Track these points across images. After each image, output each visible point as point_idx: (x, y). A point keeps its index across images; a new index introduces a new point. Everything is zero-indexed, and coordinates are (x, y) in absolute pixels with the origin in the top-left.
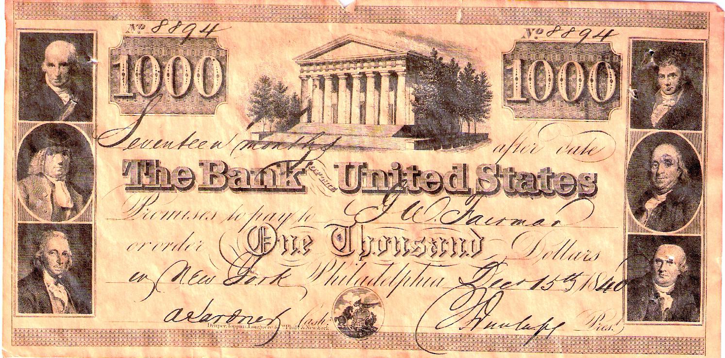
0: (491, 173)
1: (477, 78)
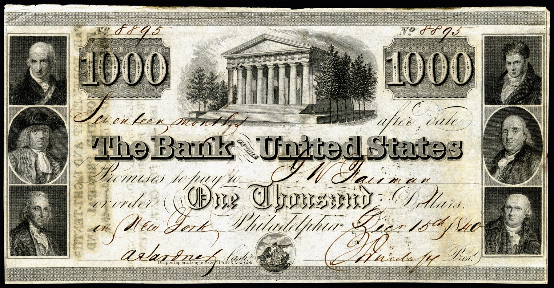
0: (379, 143)
1: (365, 67)
